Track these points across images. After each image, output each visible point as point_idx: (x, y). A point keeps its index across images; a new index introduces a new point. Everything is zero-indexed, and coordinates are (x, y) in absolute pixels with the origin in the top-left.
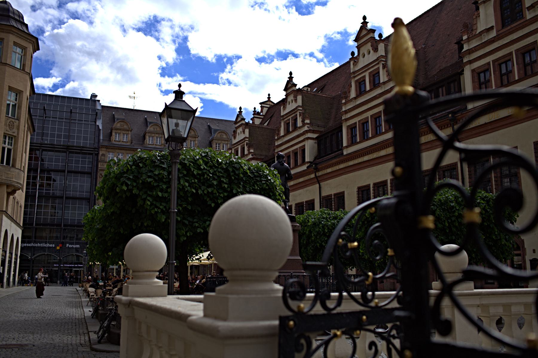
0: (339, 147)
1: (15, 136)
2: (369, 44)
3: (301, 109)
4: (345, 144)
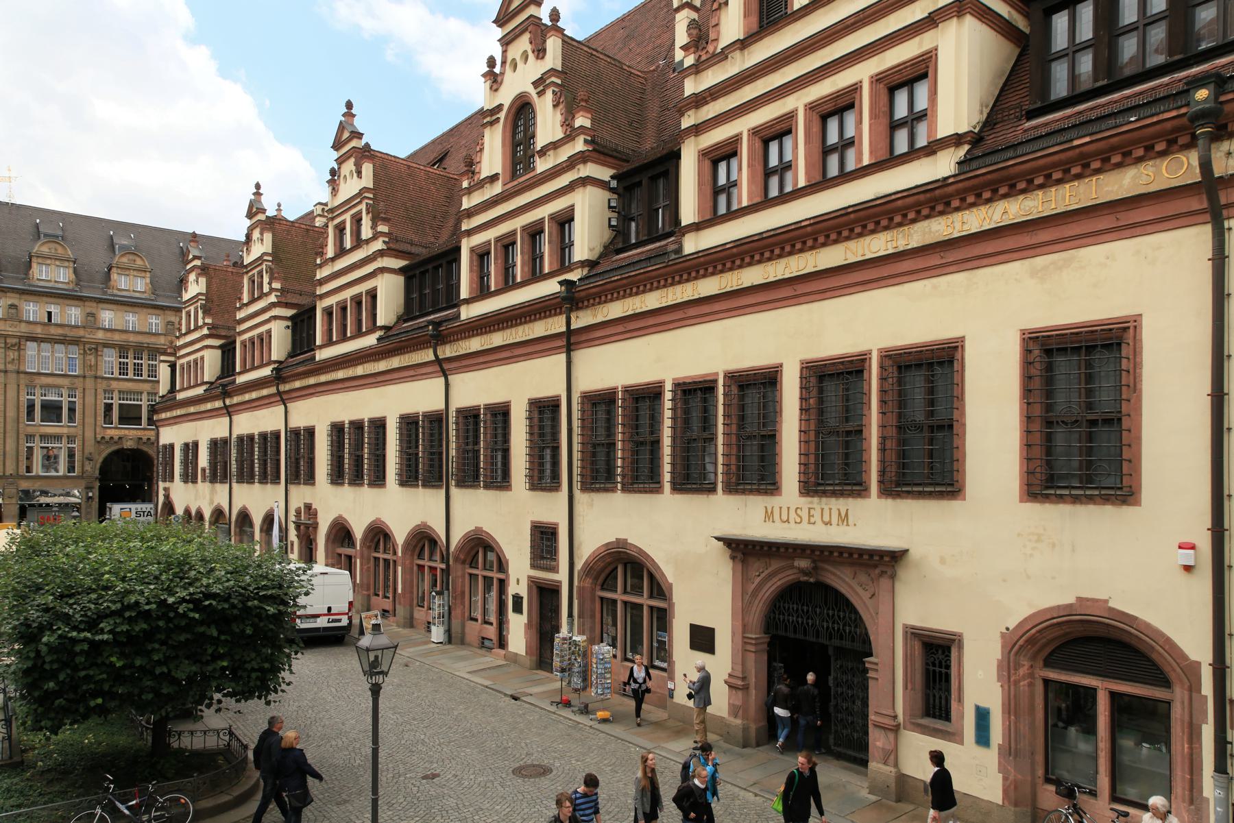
0: (453, 301)
2: (526, 38)
3: (270, 258)
4: (464, 294)
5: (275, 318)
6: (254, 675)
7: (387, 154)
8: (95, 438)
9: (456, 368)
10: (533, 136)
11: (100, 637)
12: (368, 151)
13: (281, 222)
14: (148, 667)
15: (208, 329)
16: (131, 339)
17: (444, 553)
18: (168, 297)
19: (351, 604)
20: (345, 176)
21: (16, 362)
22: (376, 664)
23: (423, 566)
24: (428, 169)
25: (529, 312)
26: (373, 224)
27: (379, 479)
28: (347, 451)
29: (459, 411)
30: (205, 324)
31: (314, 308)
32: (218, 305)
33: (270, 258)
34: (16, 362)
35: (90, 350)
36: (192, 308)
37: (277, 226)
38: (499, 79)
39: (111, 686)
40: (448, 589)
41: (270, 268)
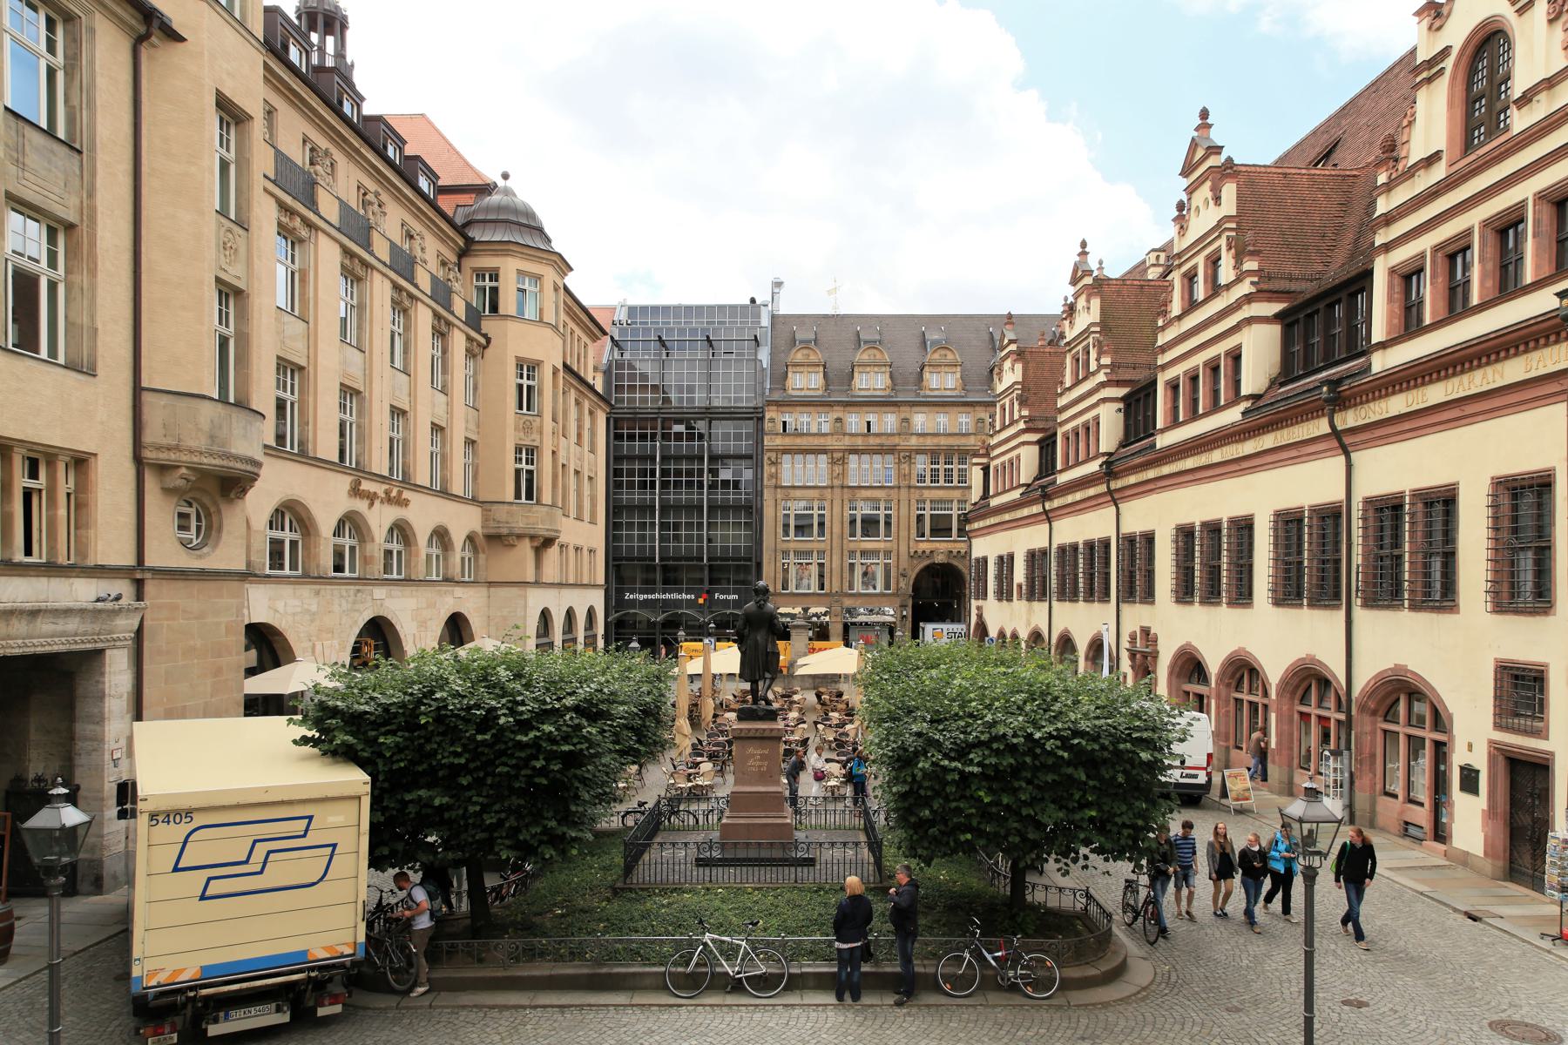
0: (1358, 347)
1: (537, 447)
3: (1098, 329)
5: (1104, 400)
6: (1126, 832)
7: (1254, 165)
8: (909, 552)
9: (1364, 442)
10: (1507, 78)
11: (971, 769)
12: (1231, 168)
13: (1111, 282)
14: (1014, 806)
15: (1025, 422)
16: (942, 443)
17: (1343, 699)
18: (978, 391)
19: (1210, 756)
21: (841, 476)
22: (1310, 840)
23: (1309, 715)
24: (1313, 172)
25: (1496, 346)
26: (1236, 262)
27: (1243, 596)
28: (1197, 560)
29: (1368, 502)
30: (1022, 417)
31: (1154, 382)
32: (1035, 394)
33: (1098, 329)
34: (841, 476)
35: (904, 458)
36: (1007, 401)
37: (1106, 288)
38: (1445, 11)
39: (979, 823)
40: (1349, 748)
41: (1098, 341)
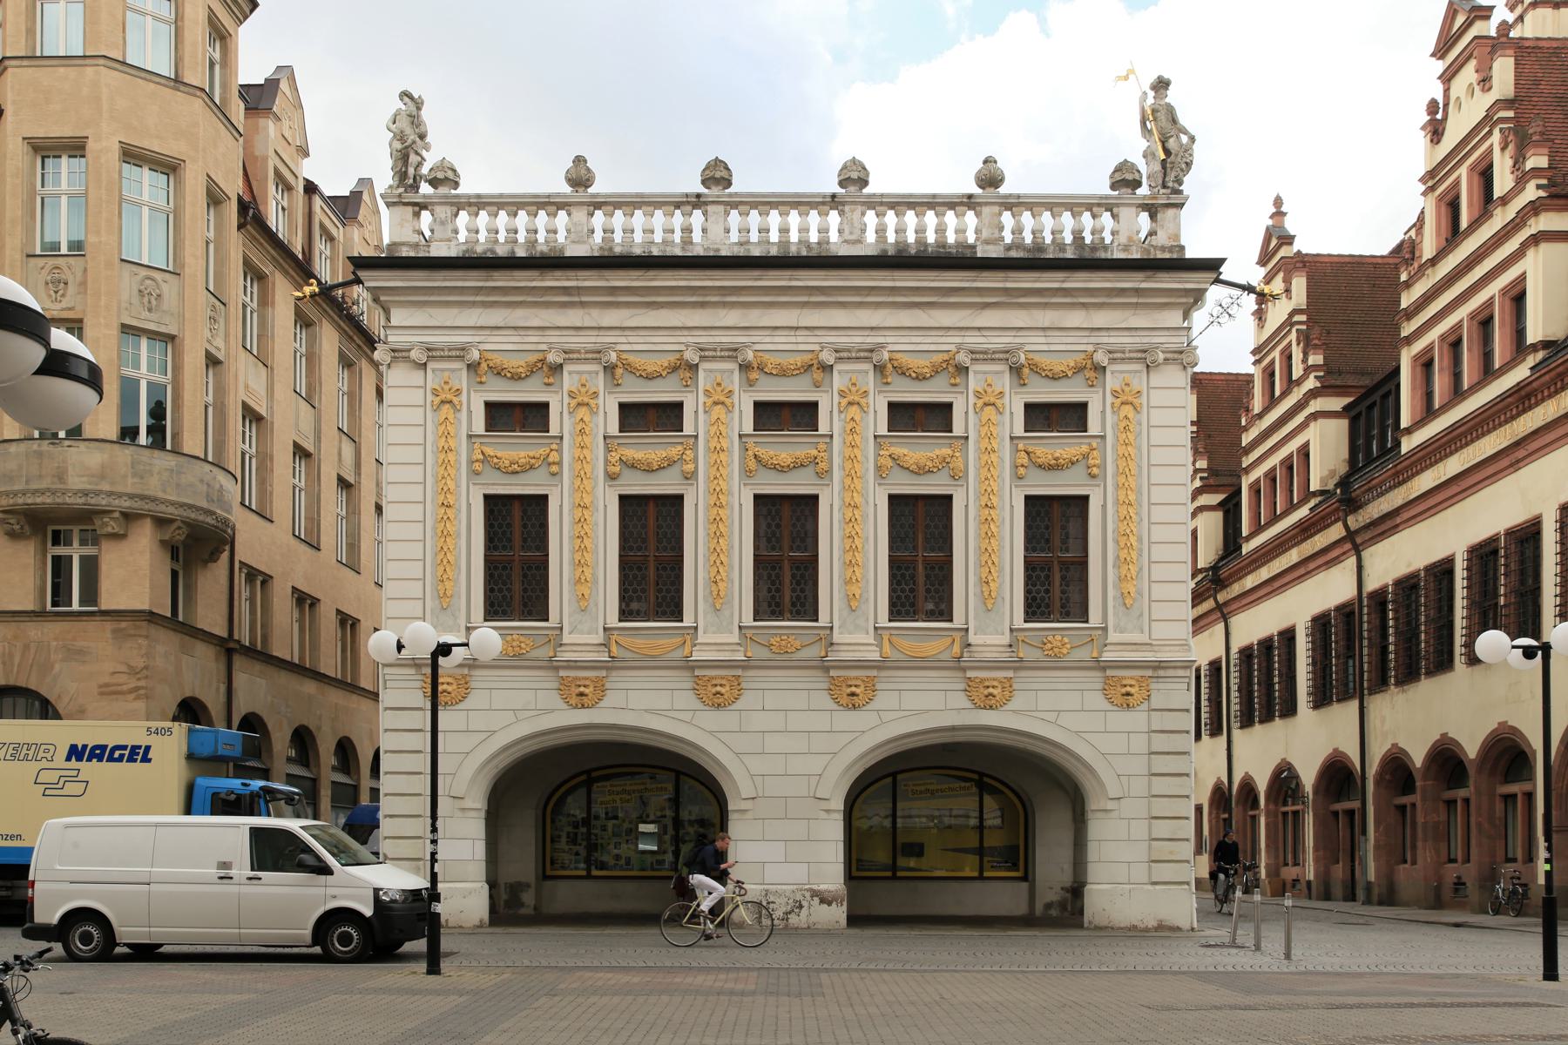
3: (1303, 318)
20: (1458, 98)
